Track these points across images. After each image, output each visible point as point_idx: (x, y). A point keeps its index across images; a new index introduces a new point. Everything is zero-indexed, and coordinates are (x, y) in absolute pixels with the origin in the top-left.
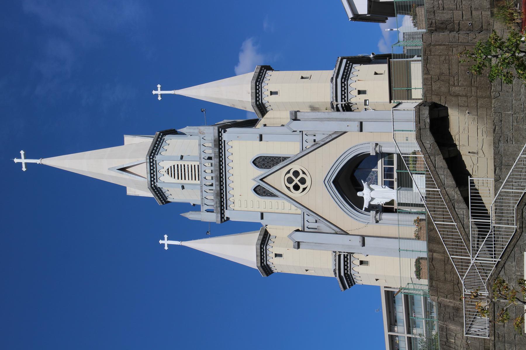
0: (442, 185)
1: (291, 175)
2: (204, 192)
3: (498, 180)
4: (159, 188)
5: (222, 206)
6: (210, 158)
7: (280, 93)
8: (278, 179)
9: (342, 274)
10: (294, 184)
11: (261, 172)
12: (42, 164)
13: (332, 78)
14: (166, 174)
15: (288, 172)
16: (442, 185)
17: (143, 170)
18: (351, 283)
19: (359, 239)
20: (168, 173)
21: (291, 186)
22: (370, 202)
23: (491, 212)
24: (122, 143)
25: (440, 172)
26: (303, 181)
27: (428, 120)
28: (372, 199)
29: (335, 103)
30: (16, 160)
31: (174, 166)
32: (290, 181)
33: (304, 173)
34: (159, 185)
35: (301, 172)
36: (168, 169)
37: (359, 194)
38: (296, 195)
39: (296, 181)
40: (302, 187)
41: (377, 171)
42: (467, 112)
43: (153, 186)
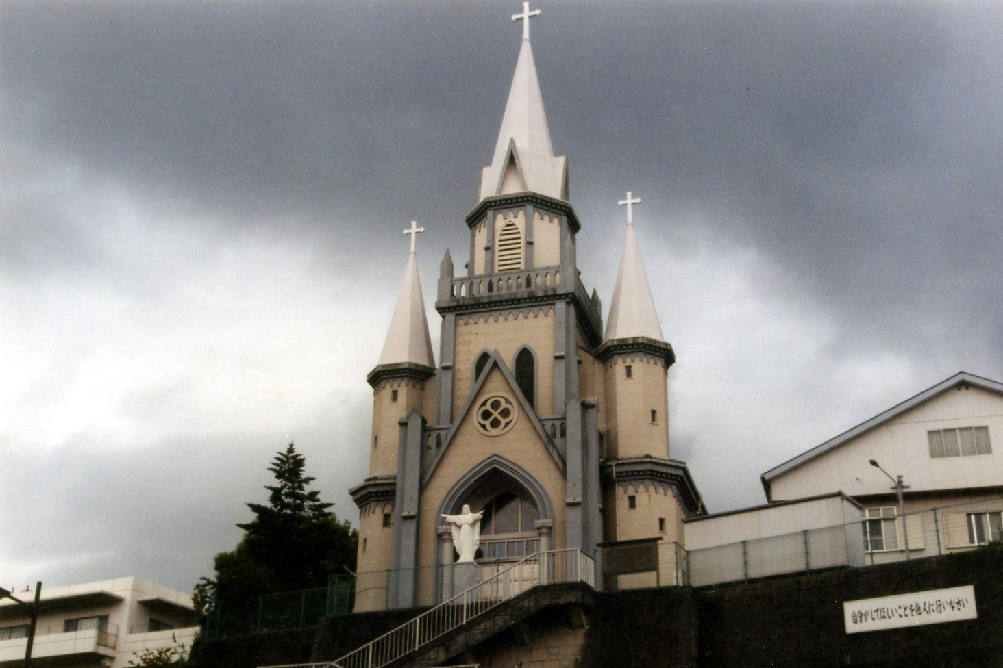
0: (470, 626)
1: (504, 405)
2: (546, 271)
4: (487, 214)
6: (529, 284)
7: (629, 381)
8: (497, 389)
9: (370, 490)
10: (492, 411)
11: (508, 359)
12: (522, 42)
13: (650, 457)
14: (507, 222)
15: (507, 401)
17: (512, 189)
18: (363, 502)
20: (508, 225)
21: (488, 407)
22: (455, 524)
24: (557, 153)
26: (495, 424)
27: (562, 601)
28: (460, 527)
29: (613, 463)
30: (526, 5)
31: (518, 233)
32: (496, 405)
33: (507, 424)
34: (490, 213)
35: (508, 420)
36: (513, 225)
37: (466, 507)
38: (476, 417)
39: (496, 414)
40: (487, 423)
41: (517, 531)
42: (579, 657)
43: (488, 204)
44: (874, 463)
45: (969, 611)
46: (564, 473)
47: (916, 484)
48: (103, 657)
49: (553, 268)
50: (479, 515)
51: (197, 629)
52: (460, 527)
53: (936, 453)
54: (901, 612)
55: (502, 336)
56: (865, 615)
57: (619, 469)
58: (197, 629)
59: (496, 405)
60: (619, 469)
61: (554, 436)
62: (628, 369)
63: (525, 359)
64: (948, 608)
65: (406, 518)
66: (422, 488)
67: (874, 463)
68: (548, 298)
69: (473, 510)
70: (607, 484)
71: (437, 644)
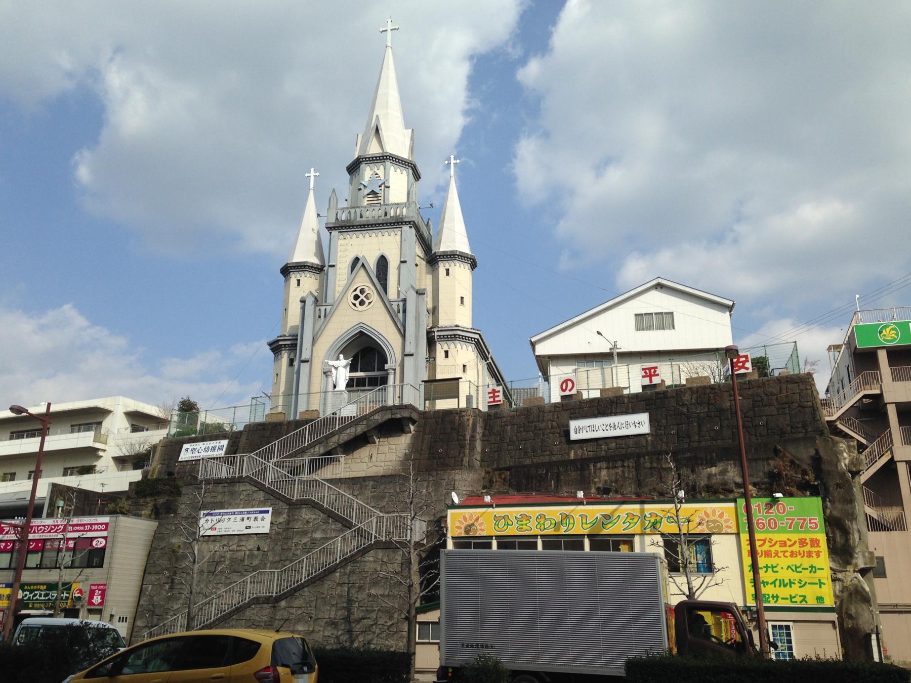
0: (341, 431)
3: (331, 481)
5: (342, 227)
6: (386, 214)
8: (362, 280)
9: (281, 343)
11: (372, 263)
16: (341, 431)
19: (406, 358)
21: (358, 292)
23: (314, 476)
25: (353, 429)
26: (362, 303)
27: (398, 416)
29: (435, 330)
34: (363, 166)
39: (362, 297)
40: (357, 302)
44: (599, 333)
45: (645, 429)
46: (403, 336)
47: (626, 346)
48: (98, 450)
49: (402, 204)
50: (349, 361)
51: (180, 460)
52: (336, 368)
53: (640, 328)
54: (604, 428)
55: (370, 246)
56: (583, 429)
57: (440, 333)
58: (180, 460)
59: (362, 291)
60: (440, 333)
61: (399, 312)
62: (448, 270)
63: (383, 262)
64: (633, 426)
65: (307, 361)
66: (314, 342)
67: (599, 333)
68: (397, 223)
69: (345, 358)
70: (431, 343)
71: (319, 442)
